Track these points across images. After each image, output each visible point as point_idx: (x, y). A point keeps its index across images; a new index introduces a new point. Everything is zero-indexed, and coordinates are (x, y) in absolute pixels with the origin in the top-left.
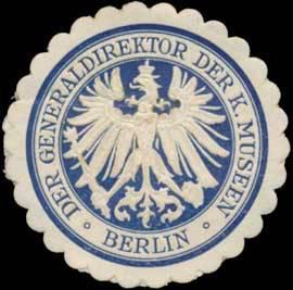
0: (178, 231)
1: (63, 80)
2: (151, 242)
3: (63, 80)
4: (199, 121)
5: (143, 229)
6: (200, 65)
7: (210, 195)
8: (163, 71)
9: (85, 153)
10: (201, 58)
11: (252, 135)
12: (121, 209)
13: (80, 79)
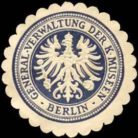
0: (83, 104)
1: (22, 63)
2: (70, 109)
3: (22, 63)
4: (92, 61)
5: (66, 103)
6: (91, 31)
7: (97, 84)
8: (76, 36)
9: (45, 68)
10: (91, 29)
11: (115, 63)
12: (57, 96)
13: (54, 28)
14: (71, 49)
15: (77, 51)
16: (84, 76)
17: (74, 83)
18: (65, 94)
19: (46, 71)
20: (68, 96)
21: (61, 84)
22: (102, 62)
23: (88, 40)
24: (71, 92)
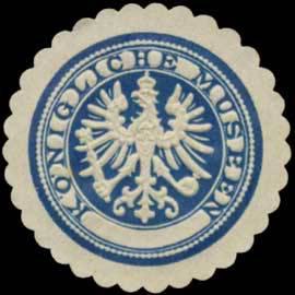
8: (165, 85)
12: (118, 208)
14: (156, 112)
15: (165, 118)
16: (176, 167)
17: (156, 187)
18: (139, 207)
19: (100, 155)
20: (145, 214)
21: (130, 190)
22: (213, 138)
23: (191, 96)
24: (152, 203)
